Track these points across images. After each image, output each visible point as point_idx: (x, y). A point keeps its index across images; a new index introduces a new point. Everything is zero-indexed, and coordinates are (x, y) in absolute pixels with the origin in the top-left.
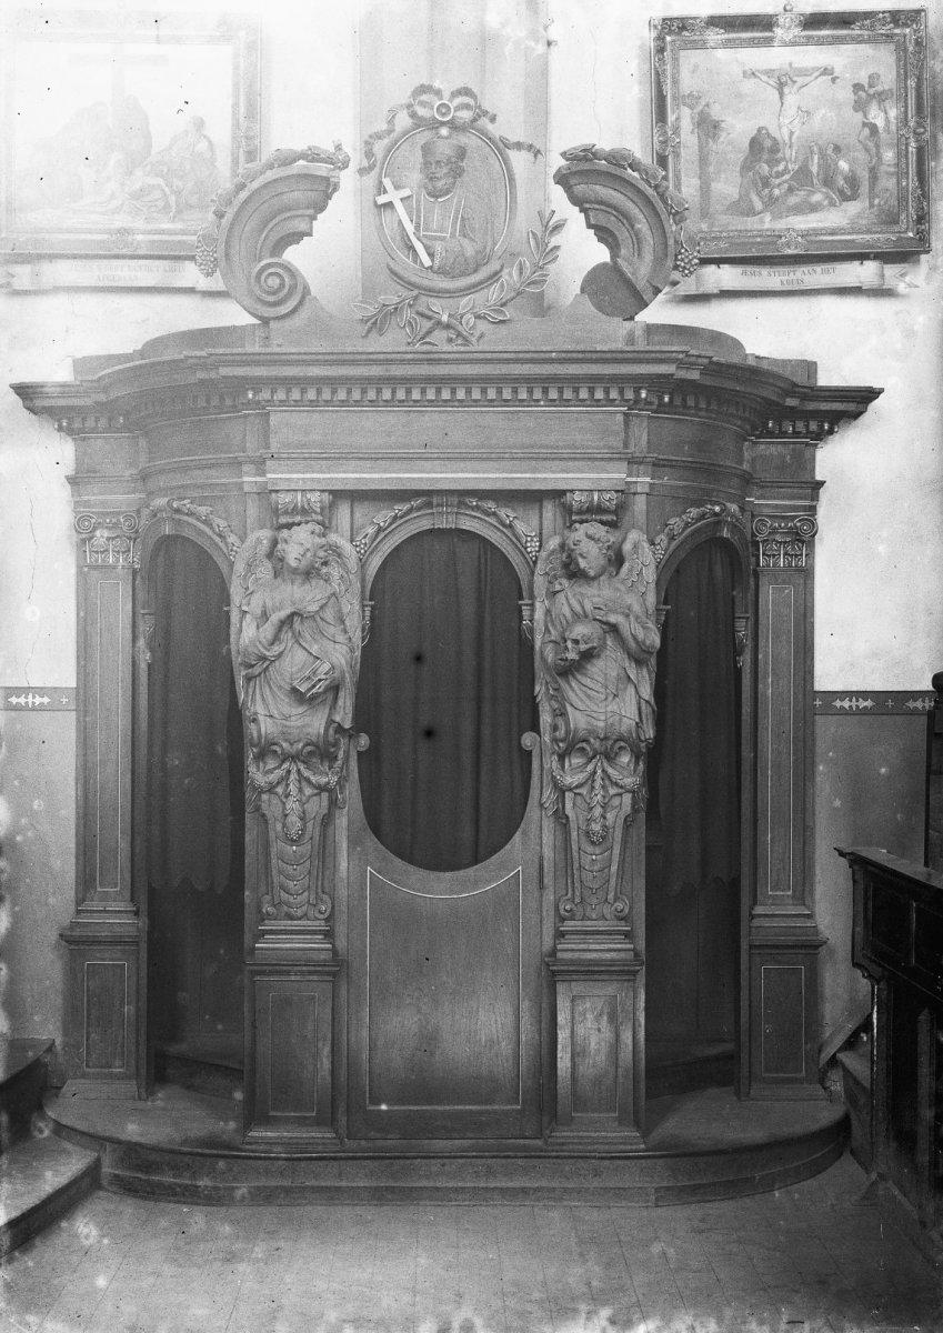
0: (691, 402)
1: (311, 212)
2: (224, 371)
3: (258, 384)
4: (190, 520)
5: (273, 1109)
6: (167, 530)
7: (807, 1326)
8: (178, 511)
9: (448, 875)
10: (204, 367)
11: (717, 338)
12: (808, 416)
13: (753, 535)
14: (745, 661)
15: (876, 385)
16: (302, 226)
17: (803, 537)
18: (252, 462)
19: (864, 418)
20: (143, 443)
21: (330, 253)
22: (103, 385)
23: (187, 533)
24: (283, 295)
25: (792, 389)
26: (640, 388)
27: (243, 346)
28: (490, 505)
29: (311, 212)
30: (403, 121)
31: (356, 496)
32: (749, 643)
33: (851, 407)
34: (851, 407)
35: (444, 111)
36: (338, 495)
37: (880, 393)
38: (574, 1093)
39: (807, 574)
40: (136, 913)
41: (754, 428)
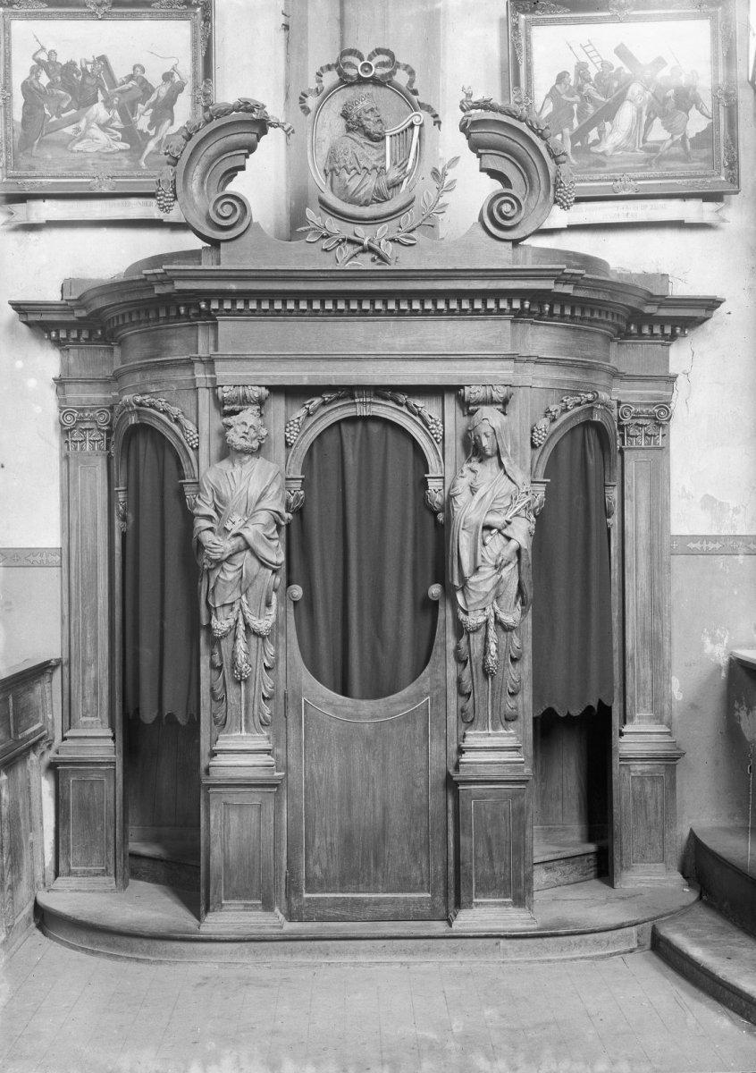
0: (557, 311)
1: (246, 151)
2: (179, 285)
3: (208, 295)
4: (163, 417)
5: (476, 897)
6: (133, 420)
7: (227, 1062)
8: (140, 404)
9: (382, 700)
10: (161, 282)
11: (586, 261)
12: (663, 321)
13: (619, 420)
14: (614, 521)
15: (719, 296)
16: (238, 162)
17: (659, 417)
18: (202, 362)
19: (708, 325)
20: (117, 350)
21: (263, 182)
22: (81, 302)
23: (147, 420)
24: (229, 220)
25: (651, 299)
26: (525, 300)
27: (200, 264)
28: (403, 398)
29: (246, 151)
30: (331, 78)
31: (294, 393)
32: (212, 437)
33: (700, 313)
34: (700, 313)
35: (367, 69)
36: (275, 390)
37: (721, 302)
38: (226, 865)
39: (664, 450)
40: (114, 738)
41: (620, 331)
